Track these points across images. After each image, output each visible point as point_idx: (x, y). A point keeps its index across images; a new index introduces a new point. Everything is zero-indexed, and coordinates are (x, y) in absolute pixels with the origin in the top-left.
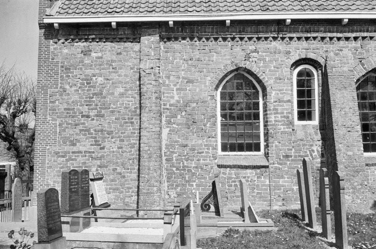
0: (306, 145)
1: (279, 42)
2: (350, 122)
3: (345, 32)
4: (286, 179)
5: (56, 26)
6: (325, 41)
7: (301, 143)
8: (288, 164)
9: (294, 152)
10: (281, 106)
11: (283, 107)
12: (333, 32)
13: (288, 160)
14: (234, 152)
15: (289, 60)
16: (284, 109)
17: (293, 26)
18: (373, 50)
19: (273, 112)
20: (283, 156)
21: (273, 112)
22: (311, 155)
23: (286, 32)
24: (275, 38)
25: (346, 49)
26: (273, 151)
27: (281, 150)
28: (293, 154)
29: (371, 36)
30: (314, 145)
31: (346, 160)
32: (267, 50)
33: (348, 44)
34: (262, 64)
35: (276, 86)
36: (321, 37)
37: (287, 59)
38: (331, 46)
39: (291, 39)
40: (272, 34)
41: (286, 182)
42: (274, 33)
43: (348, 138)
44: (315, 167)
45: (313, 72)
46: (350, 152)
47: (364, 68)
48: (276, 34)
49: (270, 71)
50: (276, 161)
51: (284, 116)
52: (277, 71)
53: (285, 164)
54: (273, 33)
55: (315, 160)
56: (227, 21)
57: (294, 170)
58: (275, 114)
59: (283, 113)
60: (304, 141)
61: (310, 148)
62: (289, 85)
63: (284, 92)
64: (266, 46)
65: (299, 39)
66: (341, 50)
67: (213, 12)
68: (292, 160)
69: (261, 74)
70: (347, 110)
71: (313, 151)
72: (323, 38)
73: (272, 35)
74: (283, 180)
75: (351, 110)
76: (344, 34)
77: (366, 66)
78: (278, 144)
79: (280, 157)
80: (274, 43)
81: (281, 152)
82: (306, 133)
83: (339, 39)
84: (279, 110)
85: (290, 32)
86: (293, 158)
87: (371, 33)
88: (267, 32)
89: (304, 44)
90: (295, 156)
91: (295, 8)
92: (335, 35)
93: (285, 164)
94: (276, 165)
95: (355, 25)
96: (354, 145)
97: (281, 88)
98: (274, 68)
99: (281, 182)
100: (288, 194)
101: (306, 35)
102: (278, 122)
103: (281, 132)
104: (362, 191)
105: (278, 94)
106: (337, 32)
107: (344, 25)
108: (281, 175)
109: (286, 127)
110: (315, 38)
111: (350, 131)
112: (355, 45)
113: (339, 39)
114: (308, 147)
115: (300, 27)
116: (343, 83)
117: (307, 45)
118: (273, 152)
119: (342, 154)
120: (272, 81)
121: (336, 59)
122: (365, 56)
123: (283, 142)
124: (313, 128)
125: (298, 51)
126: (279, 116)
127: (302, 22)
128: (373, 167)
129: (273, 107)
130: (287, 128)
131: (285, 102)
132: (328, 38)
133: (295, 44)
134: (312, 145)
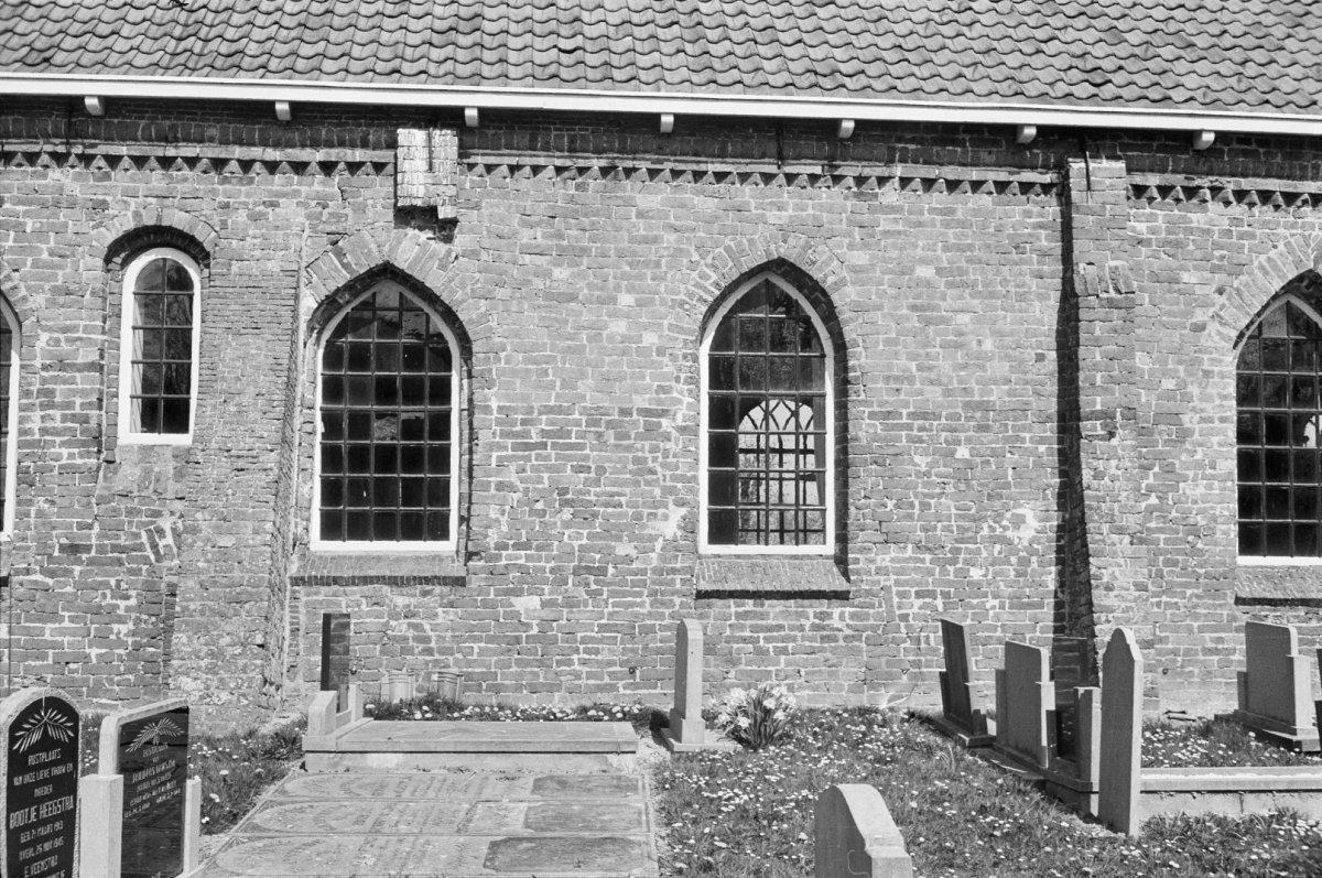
0: (139, 512)
1: (71, 171)
2: (247, 439)
3: (293, 146)
4: (66, 624)
5: (92, 106)
6: (542, 175)
7: (122, 507)
8: (76, 573)
9: (99, 537)
10: (65, 382)
11: (73, 386)
12: (252, 144)
13: (79, 562)
14: (1285, 558)
15: (103, 230)
16: (74, 393)
17: (116, 121)
18: (379, 207)
19: (37, 401)
20: (63, 548)
21: (37, 401)
22: (154, 546)
23: (94, 137)
24: (60, 159)
25: (288, 201)
26: (29, 529)
27: (54, 528)
28: (94, 541)
29: (376, 160)
30: (166, 513)
31: (207, 561)
32: (29, 198)
33: (300, 184)
34: (10, 243)
35: (60, 317)
36: (996, 183)
37: (94, 227)
38: (243, 188)
39: (113, 161)
40: (49, 143)
41: (63, 632)
42: (57, 141)
43: (230, 492)
44: (163, 586)
45: (186, 272)
46: (227, 538)
47: (343, 265)
48: (62, 143)
49: (35, 264)
50: (36, 562)
51: (74, 415)
52: (61, 267)
53: (68, 573)
54: (728, 160)
55: (166, 563)
56: (664, 119)
57: (94, 594)
58: (43, 406)
59: (69, 405)
60: (132, 499)
61: (152, 523)
62: (96, 313)
63: (80, 334)
64: (29, 181)
65: (140, 161)
66: (274, 205)
67: (404, 78)
68: (91, 562)
69: (6, 273)
70: (246, 399)
71: (161, 532)
72: (219, 164)
73: (49, 148)
74: (57, 625)
75: (260, 401)
76: (289, 150)
77: (349, 258)
78: (46, 506)
79: (50, 551)
80: (56, 174)
81: (54, 533)
82: (147, 472)
83: (272, 167)
84: (58, 394)
85: (109, 139)
86: (93, 553)
87: (377, 152)
88: (32, 136)
89: (156, 178)
90: (101, 549)
91: (721, 78)
92: (256, 152)
93: (68, 573)
94: (38, 577)
95: (322, 123)
96: (243, 513)
97: (68, 322)
98: (50, 255)
99: (47, 632)
100: (71, 672)
101: (695, 167)
102: (52, 434)
103: (61, 467)
104: (241, 662)
105: (58, 341)
106: (264, 144)
107: (1023, 144)
108: (49, 609)
109: (76, 451)
110: (192, 162)
111: (242, 470)
112: (320, 188)
113: (272, 167)
114: (144, 519)
115: (143, 123)
116: (253, 313)
117: (163, 185)
118: (29, 533)
119: (200, 544)
120: (39, 300)
121: (251, 232)
122: (349, 224)
123: (65, 502)
124: (175, 457)
125: (133, 202)
126: (57, 414)
127: (149, 106)
128: (355, 588)
129: (38, 386)
130: (81, 456)
131: (79, 371)
132: (233, 163)
133: (122, 178)
134: (157, 514)
